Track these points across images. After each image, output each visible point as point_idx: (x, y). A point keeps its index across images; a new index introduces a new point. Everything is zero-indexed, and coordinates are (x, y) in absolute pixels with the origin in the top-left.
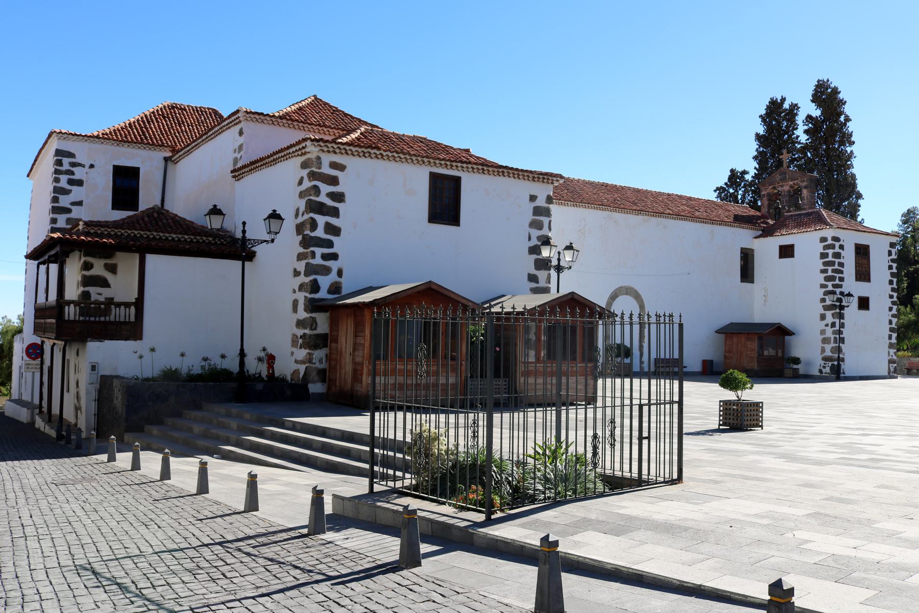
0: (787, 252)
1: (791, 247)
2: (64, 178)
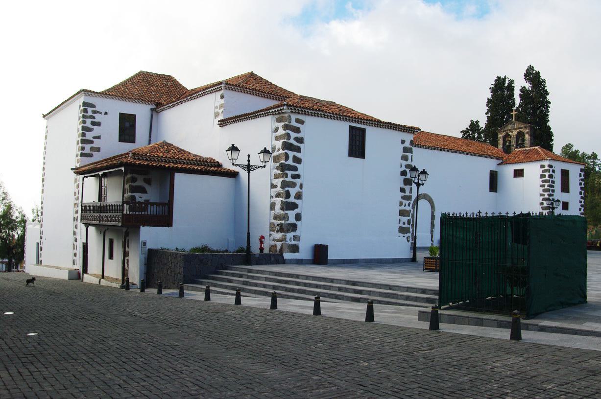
0: (519, 173)
1: (522, 170)
2: (89, 121)
